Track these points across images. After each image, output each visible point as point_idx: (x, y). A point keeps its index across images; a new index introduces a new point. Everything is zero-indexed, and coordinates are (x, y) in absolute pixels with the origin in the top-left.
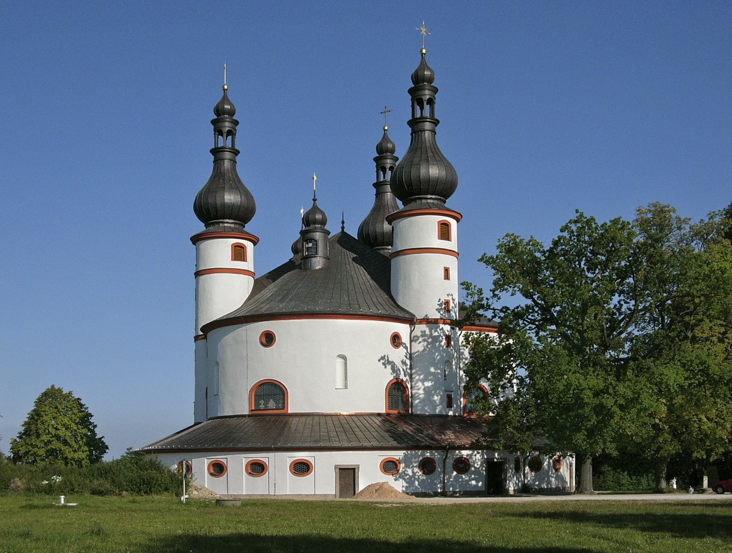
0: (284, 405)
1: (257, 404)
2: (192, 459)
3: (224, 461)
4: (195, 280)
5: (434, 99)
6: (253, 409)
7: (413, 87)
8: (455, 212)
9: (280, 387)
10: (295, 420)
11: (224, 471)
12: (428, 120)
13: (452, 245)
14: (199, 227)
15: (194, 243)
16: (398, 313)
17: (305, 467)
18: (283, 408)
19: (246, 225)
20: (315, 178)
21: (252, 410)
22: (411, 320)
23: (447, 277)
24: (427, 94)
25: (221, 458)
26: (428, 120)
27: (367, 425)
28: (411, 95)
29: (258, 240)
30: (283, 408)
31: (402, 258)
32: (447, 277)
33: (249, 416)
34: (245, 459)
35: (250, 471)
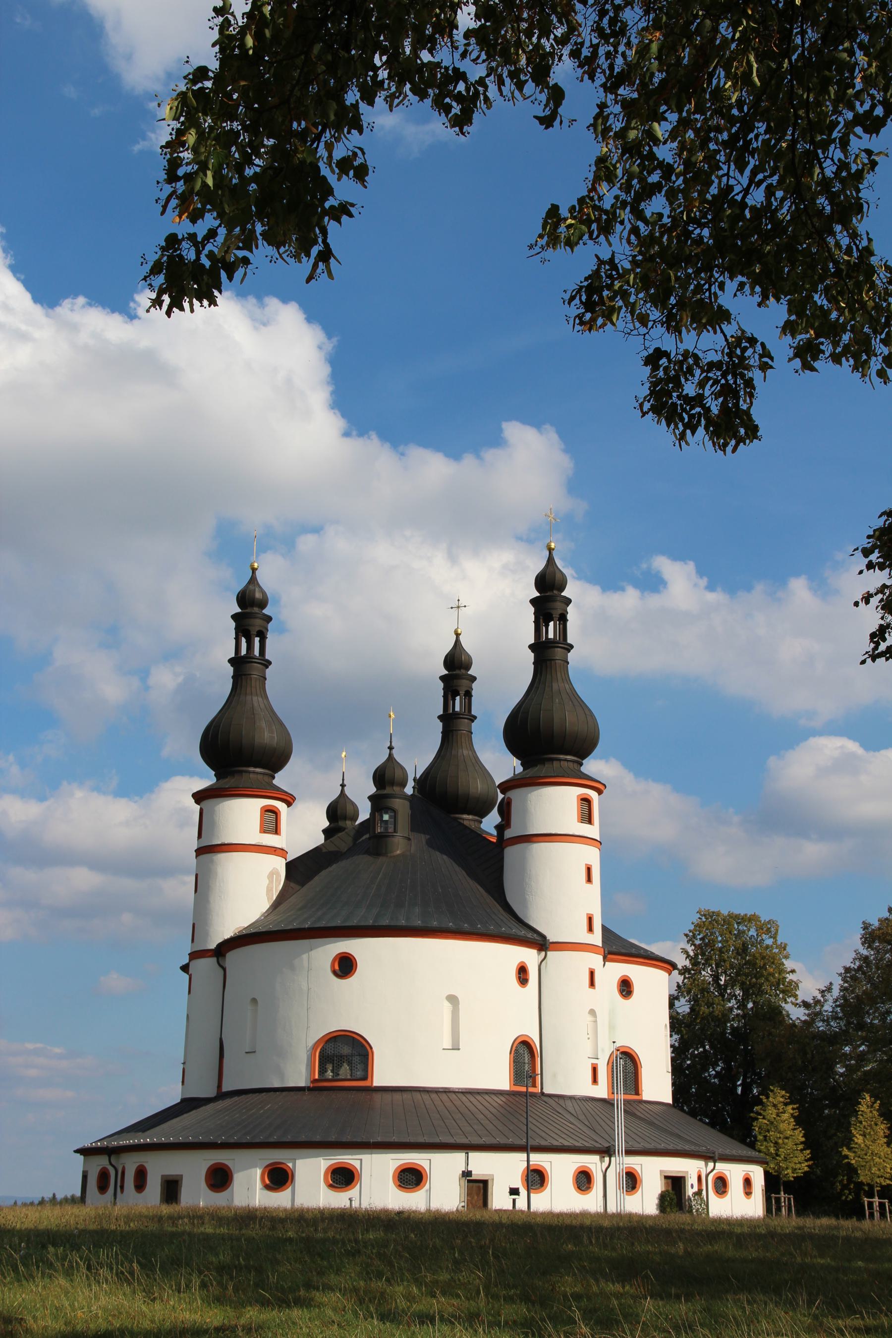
0: (367, 1073)
1: (322, 1070)
2: (295, 1159)
3: (357, 1164)
4: (195, 860)
5: (264, 630)
6: (317, 1077)
7: (537, 597)
8: (600, 782)
9: (363, 1046)
10: (377, 1097)
11: (287, 1184)
12: (560, 645)
13: (592, 831)
14: (206, 779)
15: (198, 802)
16: (523, 932)
17: (537, 1178)
18: (365, 1078)
19: (276, 775)
20: (393, 716)
21: (315, 1081)
22: (541, 944)
23: (589, 879)
24: (257, 624)
25: (539, 1159)
26: (560, 645)
27: (480, 1107)
28: (235, 621)
29: (294, 799)
30: (365, 1078)
31: (222, 857)
32: (589, 879)
33: (309, 1089)
34: (393, 1161)
35: (331, 1182)
